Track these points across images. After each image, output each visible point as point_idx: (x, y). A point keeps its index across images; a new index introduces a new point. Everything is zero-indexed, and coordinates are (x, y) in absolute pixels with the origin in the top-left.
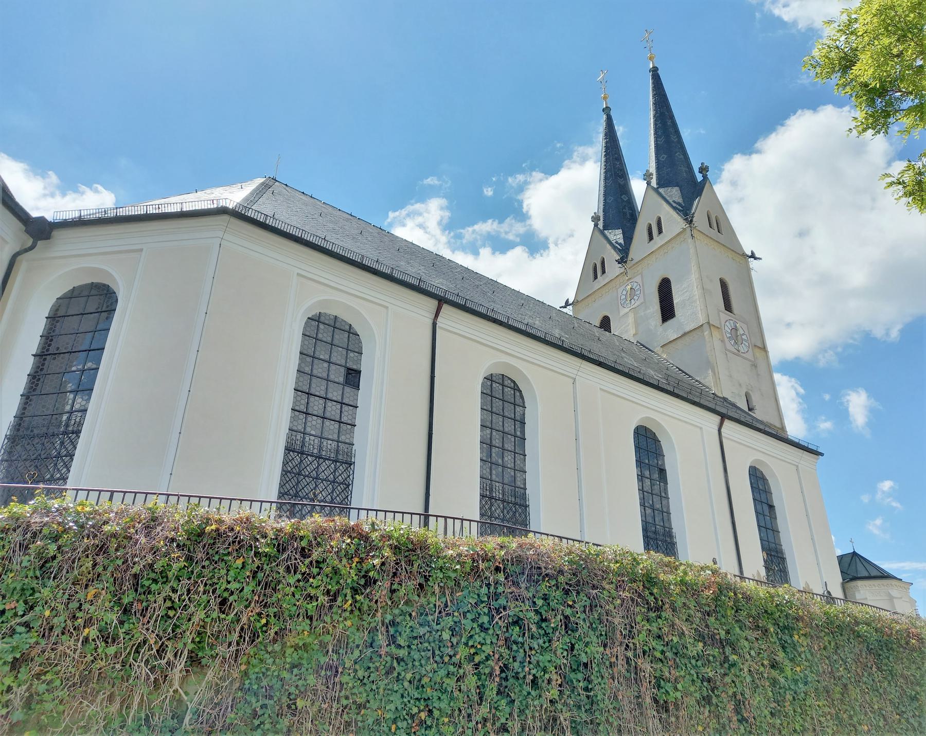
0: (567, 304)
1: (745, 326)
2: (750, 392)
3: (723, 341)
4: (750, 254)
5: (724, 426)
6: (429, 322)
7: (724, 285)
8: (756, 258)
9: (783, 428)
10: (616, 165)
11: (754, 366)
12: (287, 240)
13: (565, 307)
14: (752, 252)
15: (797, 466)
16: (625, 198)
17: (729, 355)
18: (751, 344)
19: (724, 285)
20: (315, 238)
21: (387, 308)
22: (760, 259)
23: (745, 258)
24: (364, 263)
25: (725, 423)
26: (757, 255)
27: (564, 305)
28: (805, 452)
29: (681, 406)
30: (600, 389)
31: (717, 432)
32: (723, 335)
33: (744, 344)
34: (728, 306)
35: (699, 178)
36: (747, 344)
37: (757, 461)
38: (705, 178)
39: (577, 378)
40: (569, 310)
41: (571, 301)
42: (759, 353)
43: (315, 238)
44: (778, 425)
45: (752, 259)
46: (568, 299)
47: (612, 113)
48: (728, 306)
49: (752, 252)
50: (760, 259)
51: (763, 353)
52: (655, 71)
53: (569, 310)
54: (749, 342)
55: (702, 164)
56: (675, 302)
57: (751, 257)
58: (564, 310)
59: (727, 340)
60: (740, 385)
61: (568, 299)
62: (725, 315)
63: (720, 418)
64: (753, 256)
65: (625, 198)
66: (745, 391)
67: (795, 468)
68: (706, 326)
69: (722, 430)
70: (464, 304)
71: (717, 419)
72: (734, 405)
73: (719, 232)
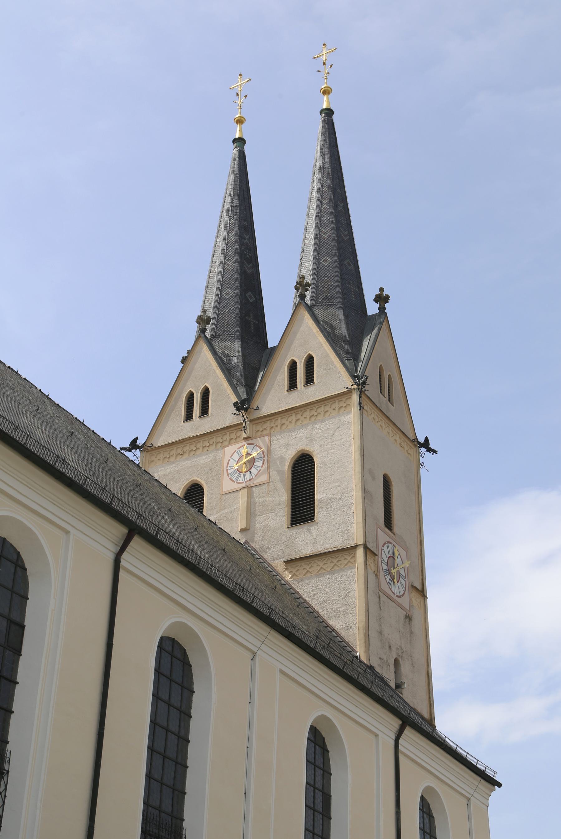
0: (134, 445)
1: (404, 553)
2: (400, 660)
3: (377, 576)
4: (422, 440)
5: (128, 549)
6: (110, 557)
7: (387, 483)
8: (429, 450)
9: (431, 723)
10: (245, 239)
11: (409, 618)
12: (351, 684)
13: (130, 450)
14: (426, 439)
15: (469, 799)
16: (251, 297)
17: (383, 598)
18: (409, 583)
19: (387, 483)
20: (47, 451)
21: (67, 532)
22: (435, 452)
23: (416, 446)
24: (56, 466)
25: (132, 543)
26: (432, 446)
27: (127, 445)
28: (482, 781)
29: (418, 741)
30: (282, 672)
31: (392, 743)
32: (378, 567)
33: (401, 583)
34: (388, 523)
35: (372, 309)
36: (404, 583)
37: (323, 718)
38: (382, 309)
39: (259, 653)
40: (134, 456)
41: (140, 442)
42: (416, 599)
43: (47, 451)
44: (426, 715)
45: (423, 450)
46: (137, 439)
47: (247, 149)
48: (388, 523)
49: (426, 439)
50: (435, 452)
51: (422, 599)
52: (328, 113)
53: (134, 456)
54: (407, 580)
55: (382, 290)
56: (317, 497)
57: (422, 445)
58: (127, 454)
59: (382, 574)
60: (390, 647)
61: (137, 439)
62: (383, 536)
63: (400, 722)
64: (426, 444)
65: (251, 297)
66: (395, 656)
67: (250, 656)
68: (360, 552)
69: (401, 741)
70: (109, 502)
71: (396, 723)
72: (382, 680)
73: (389, 401)
